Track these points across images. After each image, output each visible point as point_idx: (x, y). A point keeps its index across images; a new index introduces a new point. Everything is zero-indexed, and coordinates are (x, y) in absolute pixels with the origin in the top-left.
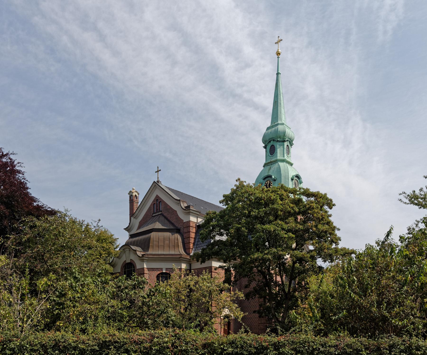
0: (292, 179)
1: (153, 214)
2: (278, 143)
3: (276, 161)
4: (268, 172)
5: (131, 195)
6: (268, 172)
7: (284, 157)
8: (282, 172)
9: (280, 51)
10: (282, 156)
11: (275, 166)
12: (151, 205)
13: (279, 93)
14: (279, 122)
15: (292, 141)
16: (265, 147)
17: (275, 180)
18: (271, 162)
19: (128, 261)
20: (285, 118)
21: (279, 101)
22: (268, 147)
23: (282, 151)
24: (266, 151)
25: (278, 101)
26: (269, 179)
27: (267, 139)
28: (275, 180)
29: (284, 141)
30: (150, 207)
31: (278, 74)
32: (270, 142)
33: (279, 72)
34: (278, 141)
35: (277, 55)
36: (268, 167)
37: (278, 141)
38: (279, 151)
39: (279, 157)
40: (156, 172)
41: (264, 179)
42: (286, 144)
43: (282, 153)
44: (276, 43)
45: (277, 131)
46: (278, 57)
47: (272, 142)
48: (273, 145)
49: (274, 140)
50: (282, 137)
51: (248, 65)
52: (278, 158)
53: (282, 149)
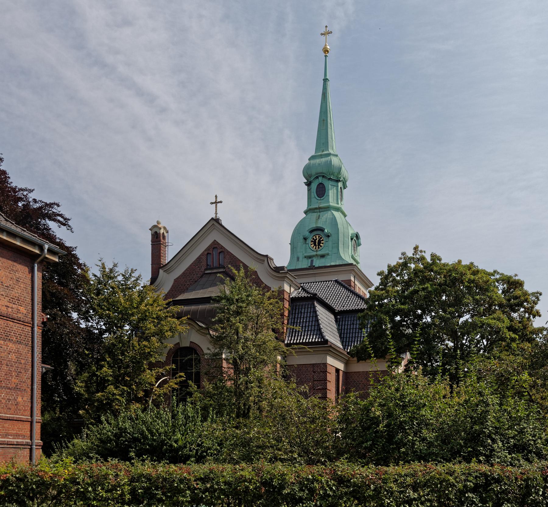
0: (352, 239)
1: (206, 269)
2: (331, 183)
3: (328, 208)
4: (316, 222)
5: (156, 232)
6: (316, 222)
7: (338, 204)
8: (339, 226)
9: (328, 47)
10: (335, 201)
11: (326, 216)
12: (202, 254)
13: (328, 109)
14: (331, 151)
15: (346, 182)
16: (308, 184)
17: (328, 236)
18: (320, 208)
19: (185, 344)
20: (335, 145)
21: (329, 121)
22: (314, 186)
23: (335, 195)
24: (309, 190)
25: (327, 120)
26: (319, 232)
27: (314, 172)
28: (328, 236)
29: (338, 181)
30: (199, 259)
31: (325, 80)
32: (317, 177)
33: (328, 77)
34: (330, 179)
35: (325, 52)
36: (315, 215)
37: (330, 179)
38: (332, 193)
39: (332, 203)
40: (212, 203)
41: (311, 231)
42: (340, 185)
43: (335, 198)
44: (322, 34)
45: (329, 164)
46: (326, 56)
47: (320, 178)
48: (321, 184)
49: (323, 176)
50: (336, 174)
51: (127, 22)
52: (331, 204)
53: (335, 191)
